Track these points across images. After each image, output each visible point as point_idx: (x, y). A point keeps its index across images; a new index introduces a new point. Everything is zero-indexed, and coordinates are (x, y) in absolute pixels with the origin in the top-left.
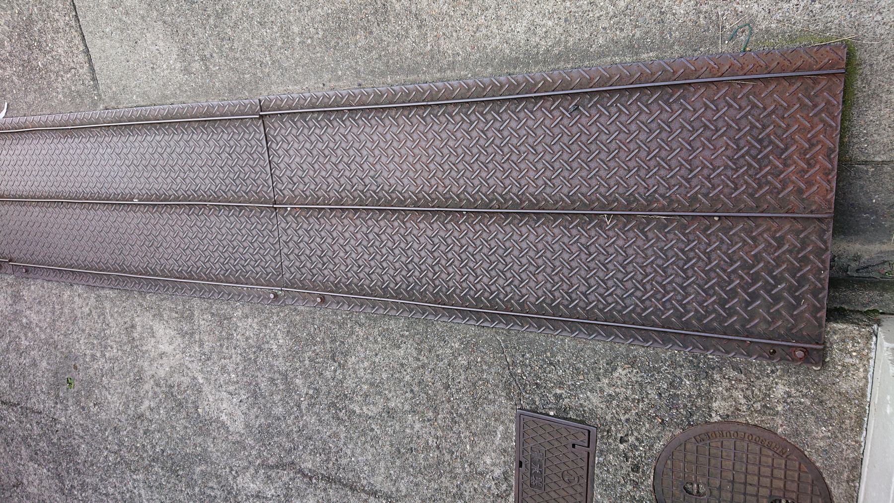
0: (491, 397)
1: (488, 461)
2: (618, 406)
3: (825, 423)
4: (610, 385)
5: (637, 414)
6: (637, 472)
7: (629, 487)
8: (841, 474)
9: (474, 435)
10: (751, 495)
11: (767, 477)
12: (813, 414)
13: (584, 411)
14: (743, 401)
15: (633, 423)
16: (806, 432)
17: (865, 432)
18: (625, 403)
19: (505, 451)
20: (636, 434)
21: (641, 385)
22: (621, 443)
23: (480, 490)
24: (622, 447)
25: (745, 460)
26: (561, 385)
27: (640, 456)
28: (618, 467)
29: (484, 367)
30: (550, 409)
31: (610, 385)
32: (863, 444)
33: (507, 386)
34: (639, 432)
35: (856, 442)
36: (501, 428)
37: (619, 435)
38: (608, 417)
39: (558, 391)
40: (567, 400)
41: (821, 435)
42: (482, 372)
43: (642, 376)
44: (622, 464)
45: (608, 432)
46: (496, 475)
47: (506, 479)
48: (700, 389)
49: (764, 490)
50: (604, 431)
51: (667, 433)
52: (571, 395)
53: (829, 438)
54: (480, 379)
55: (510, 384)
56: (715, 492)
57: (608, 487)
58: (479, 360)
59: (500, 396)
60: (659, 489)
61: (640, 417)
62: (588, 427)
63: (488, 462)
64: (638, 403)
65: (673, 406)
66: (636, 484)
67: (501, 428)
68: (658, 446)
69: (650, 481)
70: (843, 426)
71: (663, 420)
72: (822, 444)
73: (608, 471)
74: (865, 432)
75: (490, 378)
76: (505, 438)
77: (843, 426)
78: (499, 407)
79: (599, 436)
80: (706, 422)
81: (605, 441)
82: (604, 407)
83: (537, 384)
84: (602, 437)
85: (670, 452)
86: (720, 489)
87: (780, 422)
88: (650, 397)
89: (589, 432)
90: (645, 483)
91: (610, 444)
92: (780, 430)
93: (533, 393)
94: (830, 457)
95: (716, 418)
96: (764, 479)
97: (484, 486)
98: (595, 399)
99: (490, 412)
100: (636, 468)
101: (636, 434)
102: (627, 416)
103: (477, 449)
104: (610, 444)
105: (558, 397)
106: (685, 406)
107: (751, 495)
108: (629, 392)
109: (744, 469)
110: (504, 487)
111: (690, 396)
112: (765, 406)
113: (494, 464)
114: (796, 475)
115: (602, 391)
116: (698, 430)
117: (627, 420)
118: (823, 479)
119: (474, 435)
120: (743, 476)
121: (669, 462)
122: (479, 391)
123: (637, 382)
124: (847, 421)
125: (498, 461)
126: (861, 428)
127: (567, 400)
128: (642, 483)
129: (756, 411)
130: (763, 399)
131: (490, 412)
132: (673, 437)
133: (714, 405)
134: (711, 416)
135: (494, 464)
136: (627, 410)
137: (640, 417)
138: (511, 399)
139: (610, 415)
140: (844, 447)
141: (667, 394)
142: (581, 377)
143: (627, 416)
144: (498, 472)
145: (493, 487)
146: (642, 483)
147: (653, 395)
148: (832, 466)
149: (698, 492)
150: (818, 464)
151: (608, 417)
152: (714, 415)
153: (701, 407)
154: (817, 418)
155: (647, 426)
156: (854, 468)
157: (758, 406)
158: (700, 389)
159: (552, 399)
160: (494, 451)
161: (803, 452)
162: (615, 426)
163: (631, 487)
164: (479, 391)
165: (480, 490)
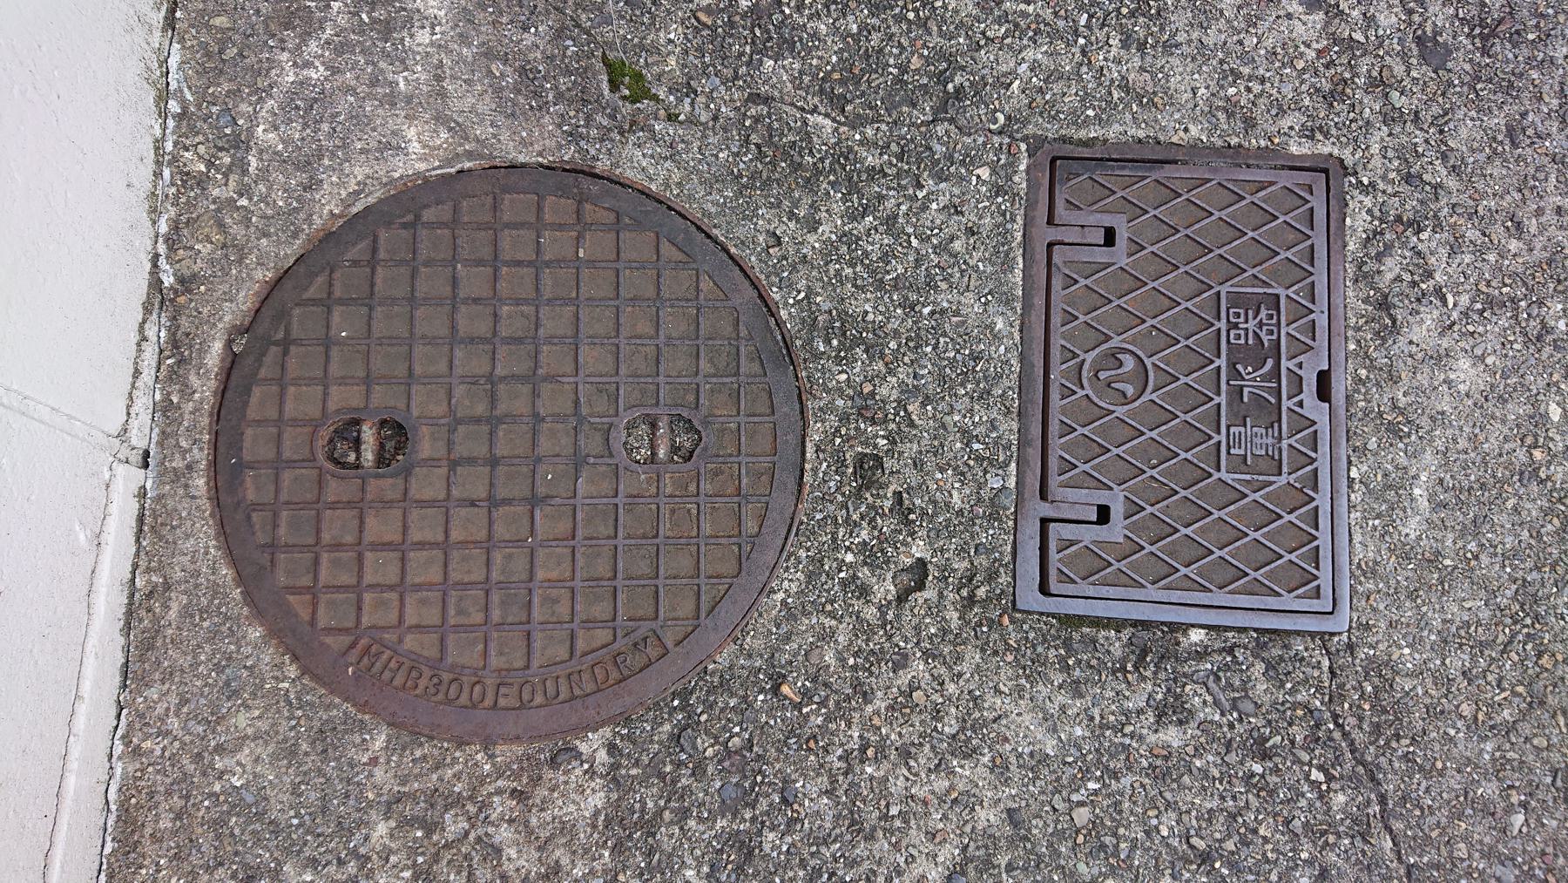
0: (1457, 661)
1: (1464, 371)
2: (937, 714)
3: (235, 802)
4: (966, 802)
5: (867, 697)
6: (861, 460)
7: (888, 390)
8: (186, 613)
9: (1530, 473)
10: (471, 461)
11: (422, 545)
12: (275, 827)
13: (1067, 669)
14: (504, 834)
15: (879, 656)
16: (292, 752)
17: (112, 796)
18: (910, 733)
19: (1393, 429)
20: (870, 613)
21: (855, 825)
22: (921, 563)
23: (1497, 231)
24: (919, 550)
25: (495, 598)
26: (1165, 768)
27: (851, 526)
28: (930, 462)
29: (1488, 789)
30: (1202, 654)
31: (966, 802)
32: (119, 748)
33: (1389, 718)
34: (862, 628)
35: (137, 752)
36: (1412, 528)
37: (930, 593)
38: (973, 657)
39: (1172, 736)
40: (1136, 701)
41: (244, 756)
42: (1499, 767)
43: (853, 863)
44: (914, 478)
45: (971, 600)
46: (1430, 316)
47: (1384, 304)
48: (650, 854)
49: (428, 494)
50: (986, 602)
51: (759, 644)
52: (1119, 729)
53: (220, 749)
54: (1511, 728)
55: (1377, 729)
56: (591, 444)
57: (967, 371)
58: (1519, 819)
59: (1416, 674)
60: (787, 409)
61: (857, 685)
62: (1051, 605)
63: (1464, 363)
64: (863, 749)
65: (740, 761)
66: (866, 407)
67: (1412, 528)
68: (790, 583)
69: (815, 435)
70: (177, 802)
71: (776, 690)
72: (242, 720)
73: (967, 436)
74: (112, 796)
75: (1464, 746)
76: (1394, 488)
77: (177, 802)
78: (1422, 622)
79: (1004, 579)
80: (628, 721)
81: (982, 561)
82: (990, 700)
83: (1265, 756)
84: (992, 576)
85: (745, 565)
86: (578, 462)
87: (379, 773)
88: (824, 781)
89: (1044, 589)
90: (833, 420)
91: (962, 551)
92: (380, 742)
93: (1281, 715)
94: (219, 669)
95: (593, 745)
96: (429, 536)
97: (1479, 252)
98: (1026, 729)
99: (1462, 589)
100: (868, 470)
101: (870, 613)
102: (904, 678)
103: (1517, 409)
104: (962, 551)
105: (1171, 710)
106: (698, 771)
107: (471, 461)
108: (897, 786)
109: (498, 557)
110: (1391, 267)
111: (684, 814)
112: (430, 828)
113: (1440, 359)
114: (324, 575)
115: (999, 768)
116: (652, 684)
117: (901, 662)
118: (240, 579)
119: (1530, 473)
120: (500, 530)
121: (751, 526)
122: (1511, 675)
123: (871, 837)
124: (165, 823)
125: (1423, 379)
126: (124, 806)
127: (1136, 701)
128: (844, 418)
129: (457, 802)
130: (436, 858)
131: (1462, 589)
132: (735, 635)
133: (597, 800)
134: (612, 748)
135: (1440, 359)
136: (903, 705)
137: (857, 685)
138: (1374, 667)
139: (965, 667)
140: (174, 723)
141: (763, 805)
142: (1082, 816)
143: (904, 678)
144: (1422, 329)
145: (1439, 261)
146: (844, 418)
147: (810, 789)
148: (214, 635)
149: (654, 426)
150: (255, 633)
151: (973, 657)
152: (602, 756)
153: (643, 780)
154: (260, 815)
155: (830, 658)
156: (147, 646)
157: (454, 825)
158: (650, 854)
159: (1195, 696)
160: (1439, 418)
161: (304, 671)
162: (945, 631)
163: (883, 391)
164: (1511, 675)
165: (1497, 231)
